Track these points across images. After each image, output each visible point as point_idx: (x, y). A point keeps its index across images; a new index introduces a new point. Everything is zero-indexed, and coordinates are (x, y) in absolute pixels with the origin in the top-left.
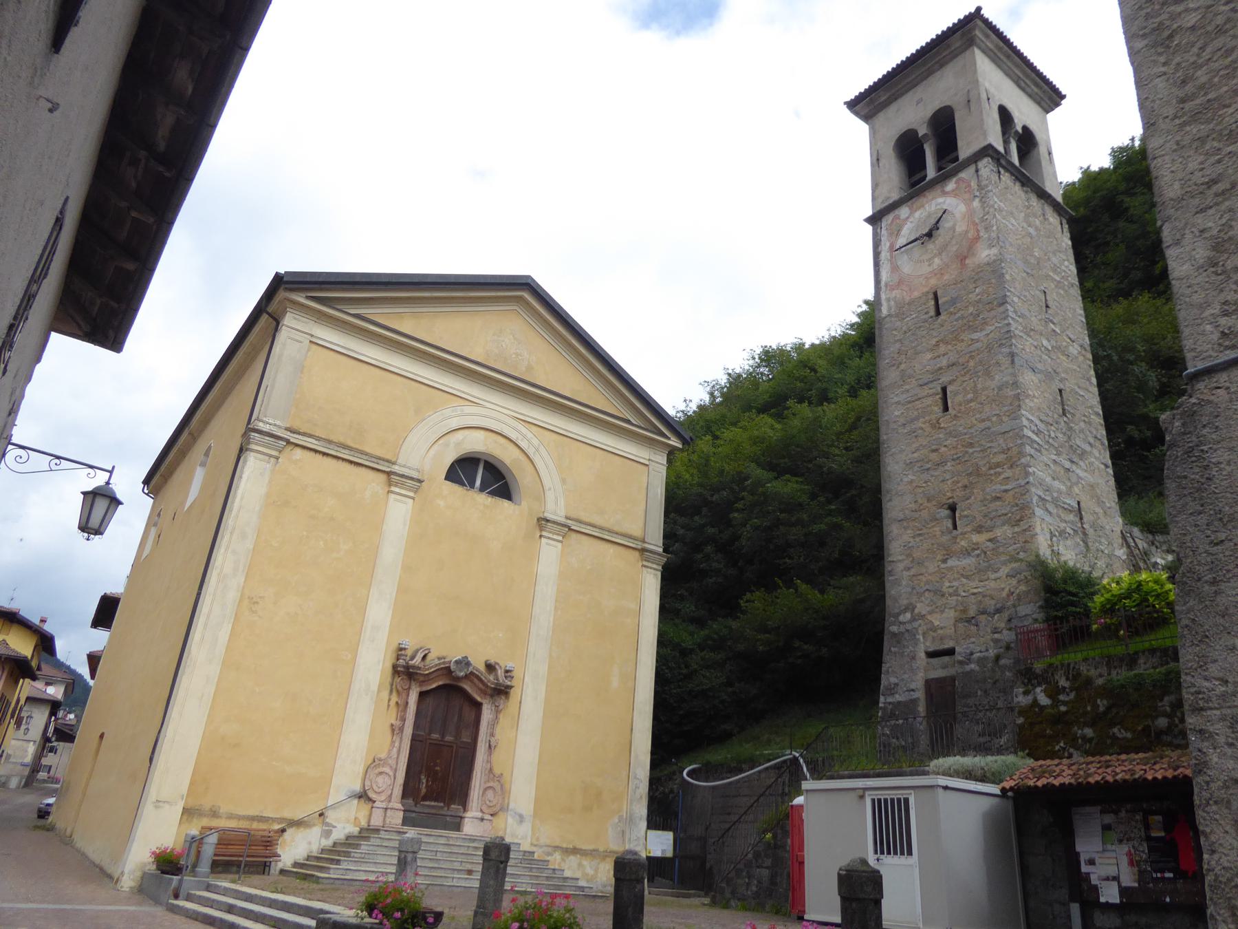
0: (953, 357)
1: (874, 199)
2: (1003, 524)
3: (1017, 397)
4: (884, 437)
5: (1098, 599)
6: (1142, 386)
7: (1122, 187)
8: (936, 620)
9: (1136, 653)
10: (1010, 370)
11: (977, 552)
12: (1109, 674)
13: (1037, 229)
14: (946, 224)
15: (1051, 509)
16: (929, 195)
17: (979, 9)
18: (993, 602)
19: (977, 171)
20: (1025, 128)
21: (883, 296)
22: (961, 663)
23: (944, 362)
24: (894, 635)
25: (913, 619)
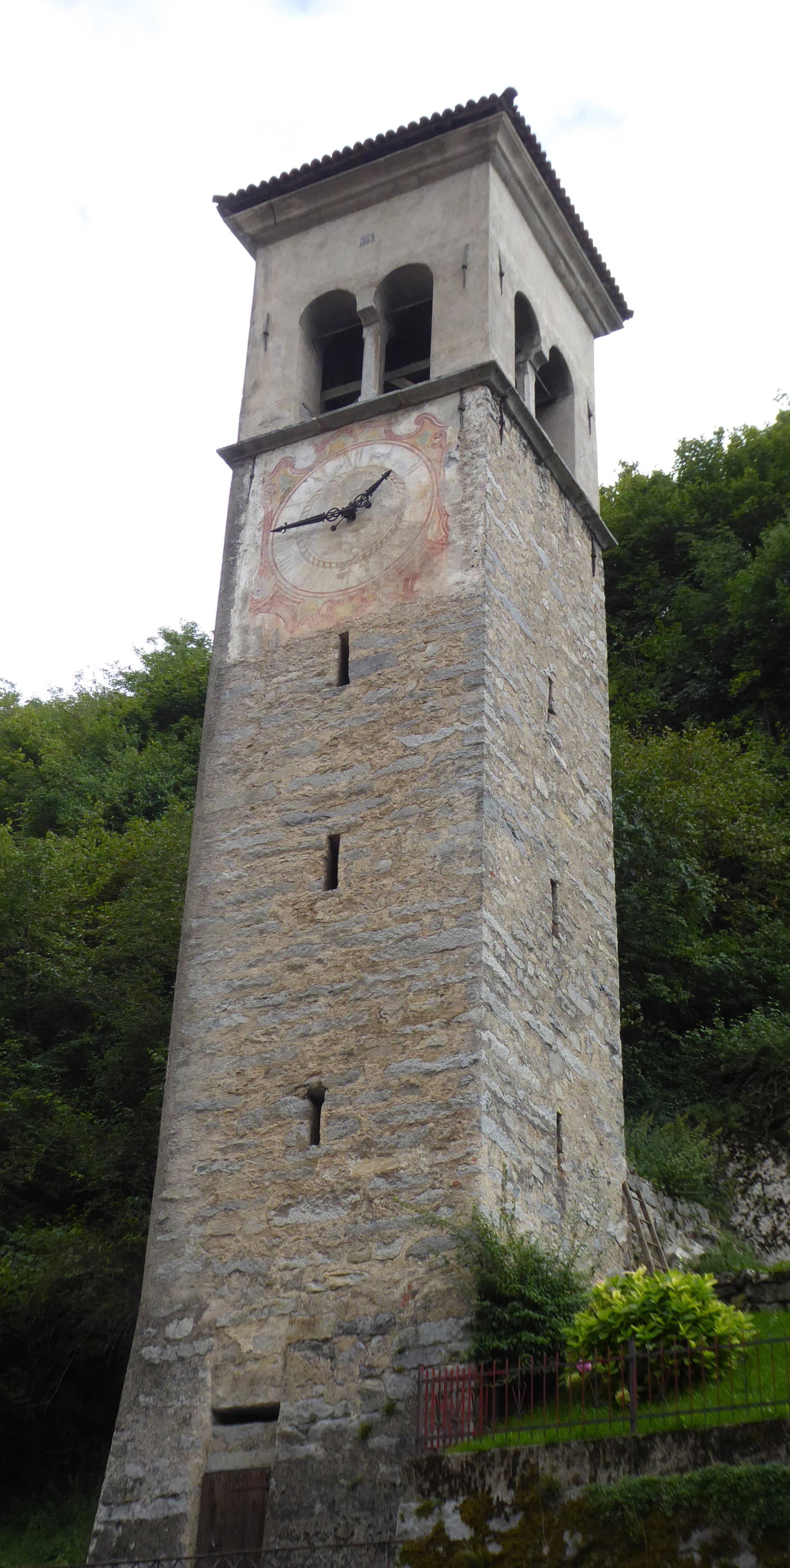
0: (362, 776)
1: (245, 412)
2: (414, 1145)
3: (478, 880)
4: (191, 923)
5: (583, 1320)
6: (685, 900)
7: (693, 517)
8: (247, 1340)
9: (650, 1437)
10: (472, 824)
11: (356, 1197)
12: (593, 1479)
13: (551, 553)
14: (385, 500)
15: (510, 1123)
16: (363, 433)
17: (510, 94)
18: (372, 1309)
19: (461, 409)
20: (555, 352)
21: (235, 621)
22: (288, 1438)
23: (342, 783)
24: (150, 1366)
25: (197, 1335)
